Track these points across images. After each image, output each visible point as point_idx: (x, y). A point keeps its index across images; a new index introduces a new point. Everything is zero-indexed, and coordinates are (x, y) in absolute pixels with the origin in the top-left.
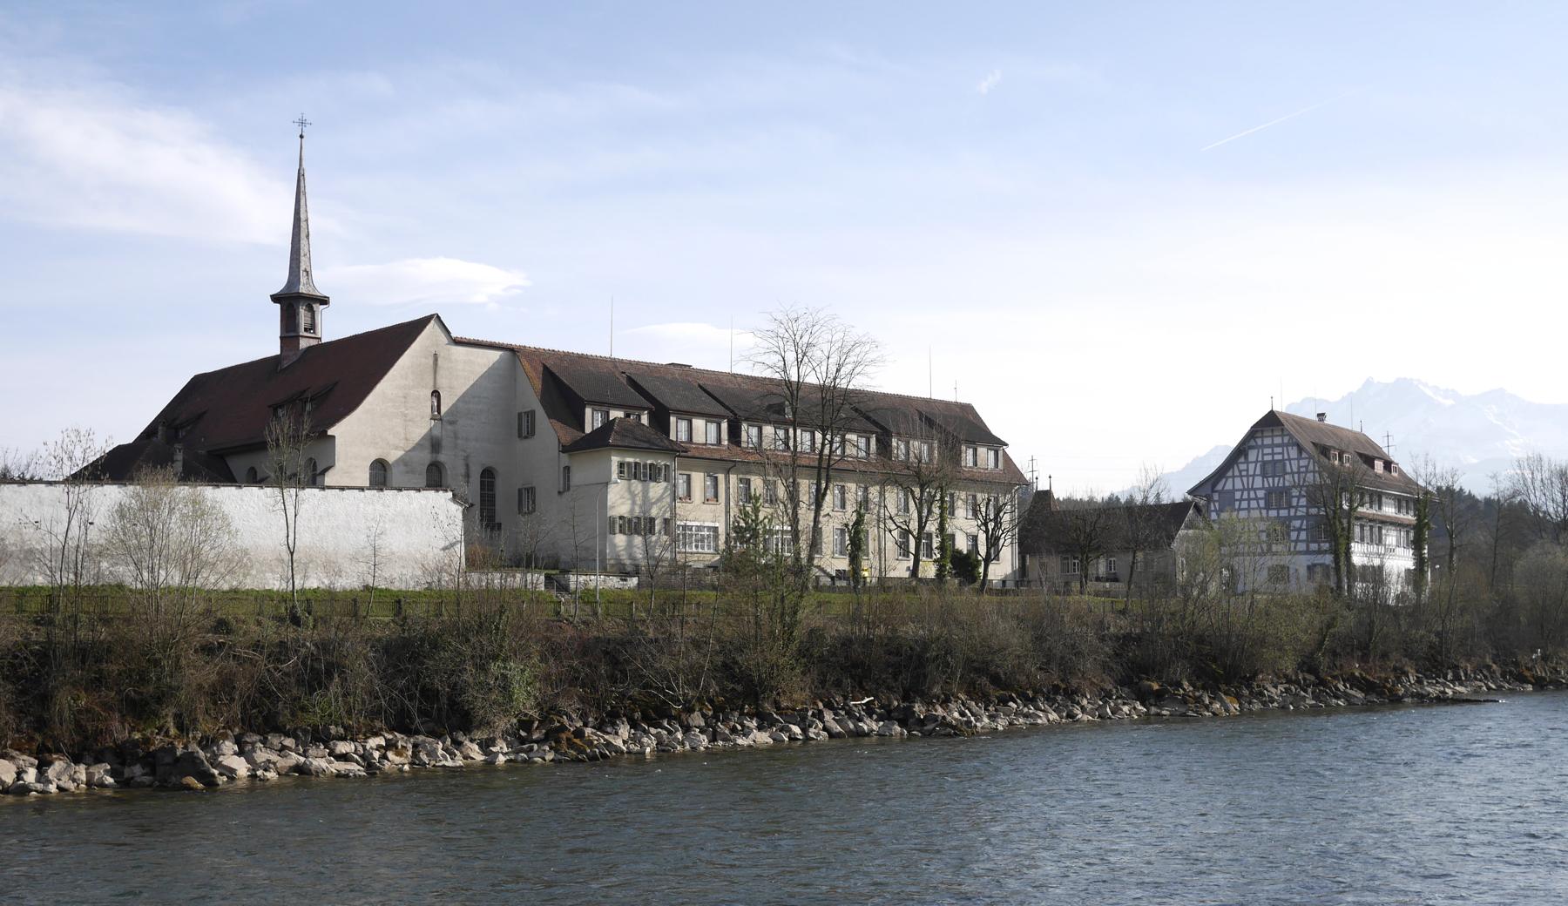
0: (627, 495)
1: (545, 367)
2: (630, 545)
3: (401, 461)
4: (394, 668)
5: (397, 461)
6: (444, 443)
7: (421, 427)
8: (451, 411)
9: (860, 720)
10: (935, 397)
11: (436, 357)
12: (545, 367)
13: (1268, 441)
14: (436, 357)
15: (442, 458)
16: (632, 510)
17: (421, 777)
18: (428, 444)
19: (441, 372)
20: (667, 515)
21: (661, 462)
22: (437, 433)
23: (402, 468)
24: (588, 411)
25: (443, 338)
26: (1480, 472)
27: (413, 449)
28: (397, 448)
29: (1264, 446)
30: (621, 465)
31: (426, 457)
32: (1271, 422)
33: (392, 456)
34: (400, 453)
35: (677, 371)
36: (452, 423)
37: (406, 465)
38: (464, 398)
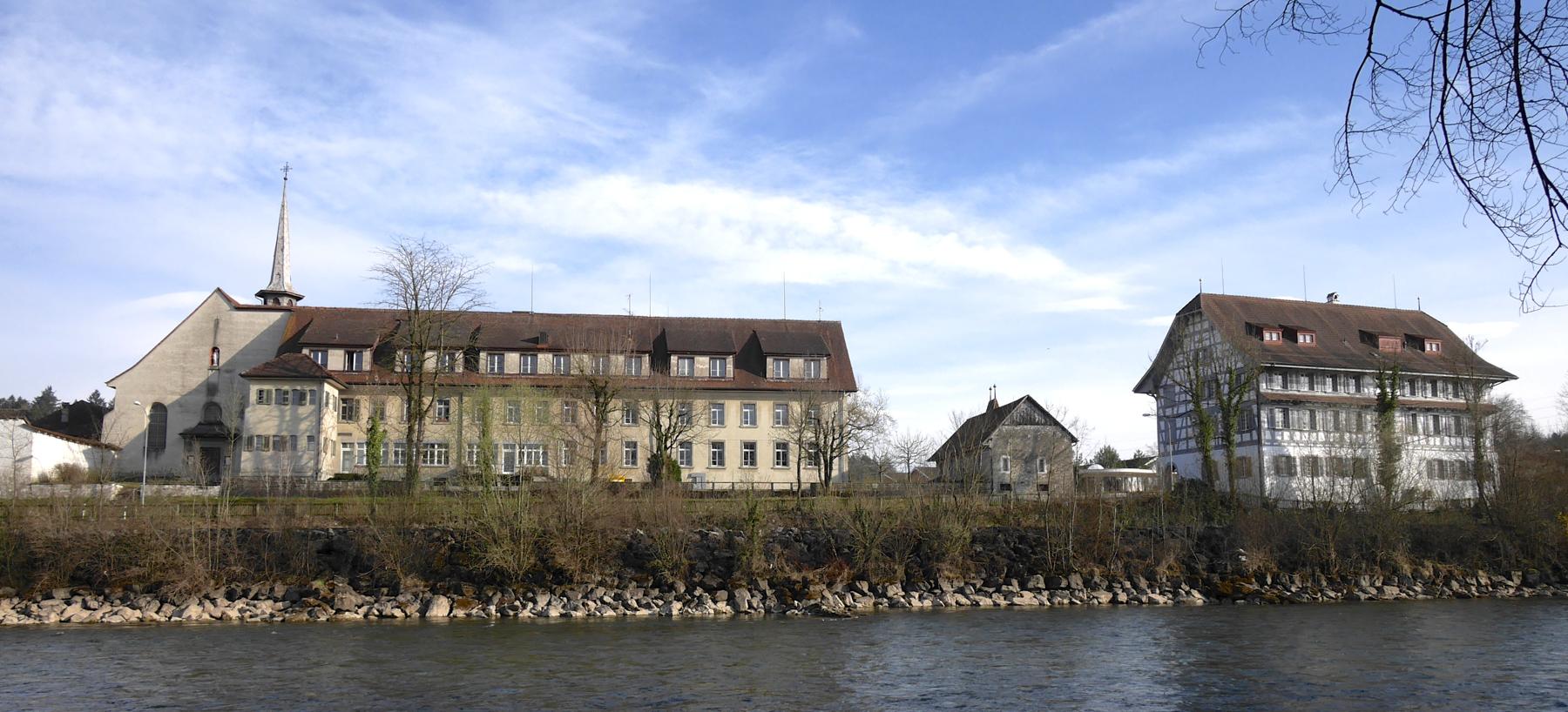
3: (178, 403)
5: (173, 404)
7: (199, 376)
8: (229, 363)
9: (1143, 592)
10: (1228, 293)
11: (217, 322)
13: (1198, 327)
14: (217, 322)
15: (217, 399)
17: (92, 633)
21: (307, 388)
22: (214, 380)
25: (225, 306)
28: (173, 393)
29: (1195, 333)
31: (202, 399)
32: (1192, 311)
33: (168, 400)
34: (176, 397)
36: (228, 371)
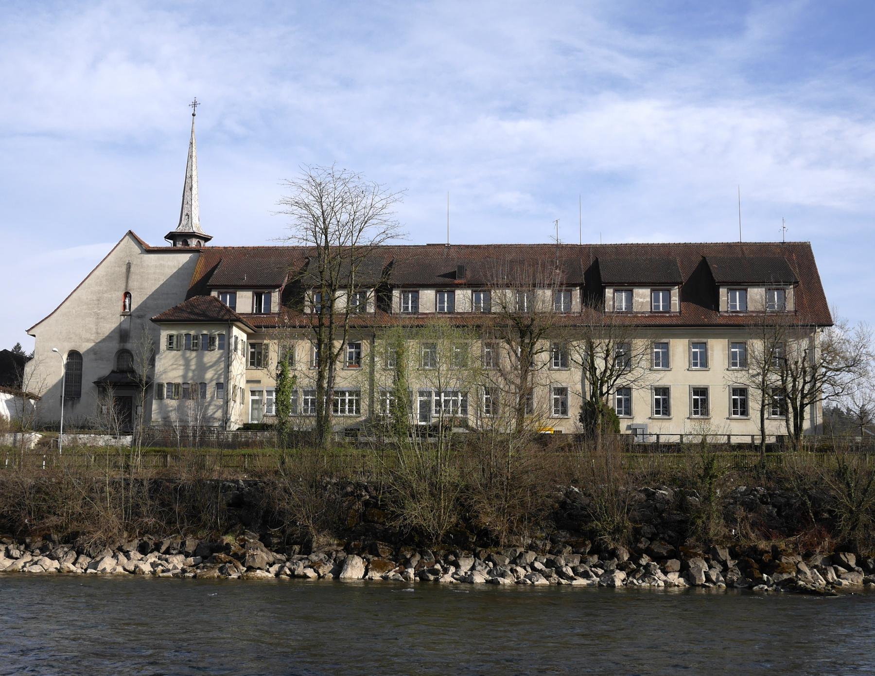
0: (182, 362)
1: (596, 262)
2: (180, 409)
3: (92, 351)
4: (665, 508)
5: (88, 351)
6: (132, 334)
7: (111, 322)
11: (129, 266)
12: (596, 262)
14: (129, 266)
16: (184, 376)
18: (117, 336)
19: (133, 277)
20: (222, 381)
23: (92, 356)
24: (723, 291)
25: (136, 249)
26: (218, 241)
27: (104, 340)
28: (88, 340)
30: (171, 337)
31: (115, 346)
34: (91, 345)
35: (453, 253)
36: (139, 317)
37: (95, 354)
38: (152, 297)
